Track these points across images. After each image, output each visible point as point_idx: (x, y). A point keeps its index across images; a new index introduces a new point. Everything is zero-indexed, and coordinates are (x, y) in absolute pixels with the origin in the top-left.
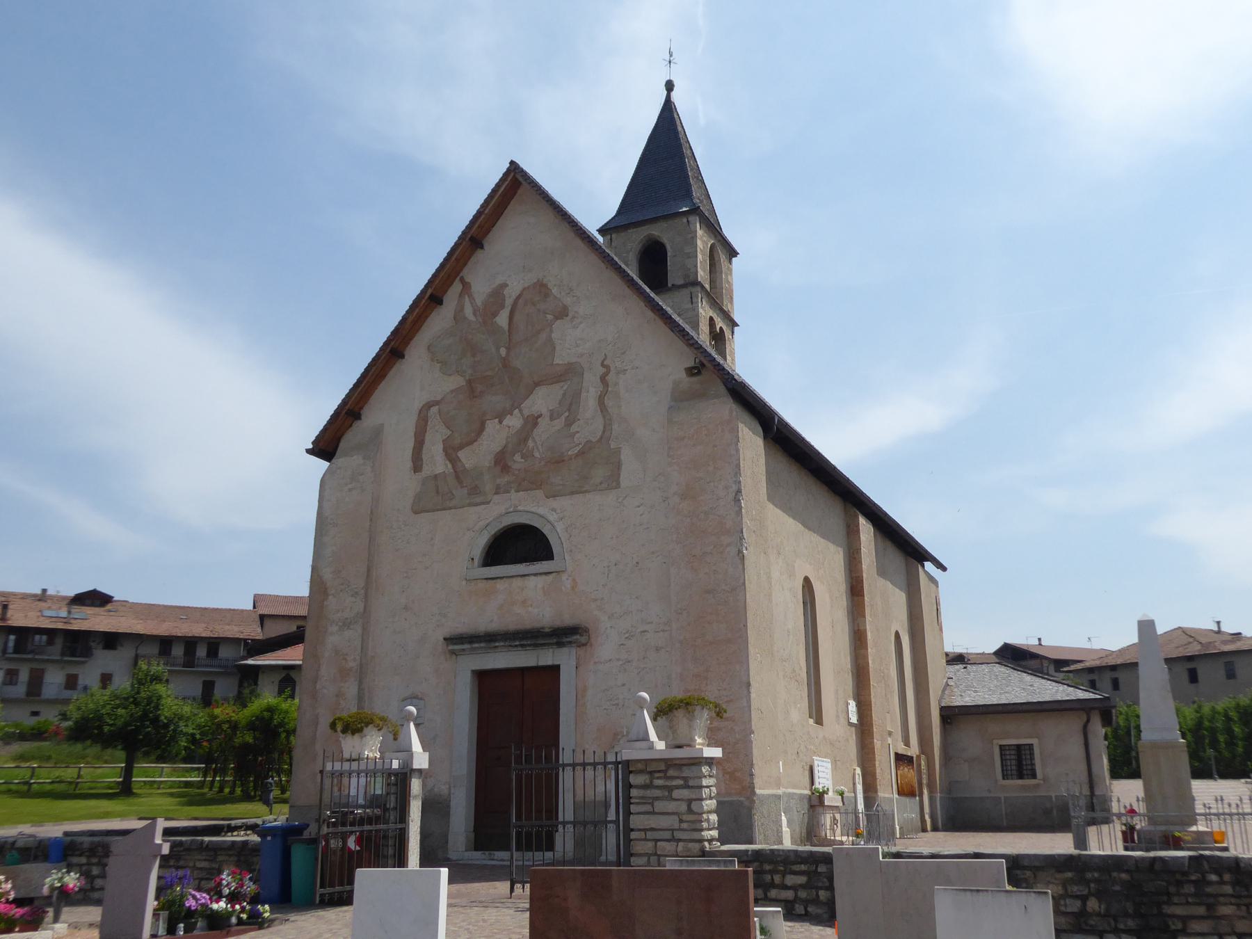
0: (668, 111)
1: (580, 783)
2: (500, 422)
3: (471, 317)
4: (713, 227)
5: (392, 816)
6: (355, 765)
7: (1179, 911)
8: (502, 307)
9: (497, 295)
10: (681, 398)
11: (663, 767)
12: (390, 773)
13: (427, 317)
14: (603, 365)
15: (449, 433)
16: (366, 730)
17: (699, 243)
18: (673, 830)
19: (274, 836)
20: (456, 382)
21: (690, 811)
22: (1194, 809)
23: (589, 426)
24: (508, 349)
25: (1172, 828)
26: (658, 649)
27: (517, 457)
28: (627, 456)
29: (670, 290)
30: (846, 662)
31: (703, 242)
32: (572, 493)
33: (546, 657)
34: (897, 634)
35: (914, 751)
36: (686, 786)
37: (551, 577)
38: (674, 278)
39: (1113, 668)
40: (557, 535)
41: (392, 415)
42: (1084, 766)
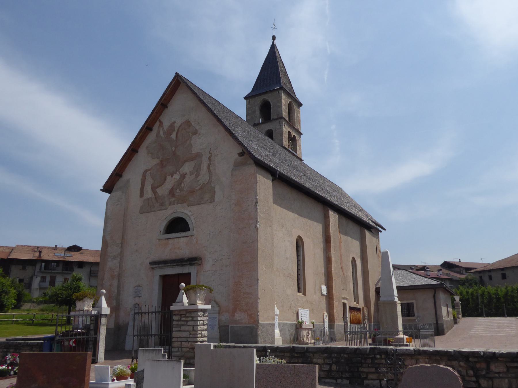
0: (273, 48)
1: (150, 318)
2: (172, 177)
3: (162, 136)
4: (291, 95)
5: (92, 333)
6: (81, 313)
7: (365, 370)
8: (174, 131)
9: (172, 127)
10: (237, 165)
11: (185, 313)
12: (92, 316)
13: (146, 136)
14: (209, 153)
15: (153, 181)
16: (85, 299)
17: (283, 101)
18: (187, 338)
19: (48, 340)
20: (156, 161)
21: (194, 330)
22: (398, 328)
23: (204, 178)
24: (176, 148)
25: (386, 336)
26: (226, 266)
27: (178, 191)
28: (217, 189)
29: (271, 121)
30: (321, 269)
31: (285, 100)
32: (197, 204)
33: (186, 270)
34: (353, 259)
35: (361, 305)
36: (192, 320)
37: (188, 238)
38: (273, 116)
39: (489, 271)
40: (191, 221)
41: (133, 176)
42: (433, 312)
